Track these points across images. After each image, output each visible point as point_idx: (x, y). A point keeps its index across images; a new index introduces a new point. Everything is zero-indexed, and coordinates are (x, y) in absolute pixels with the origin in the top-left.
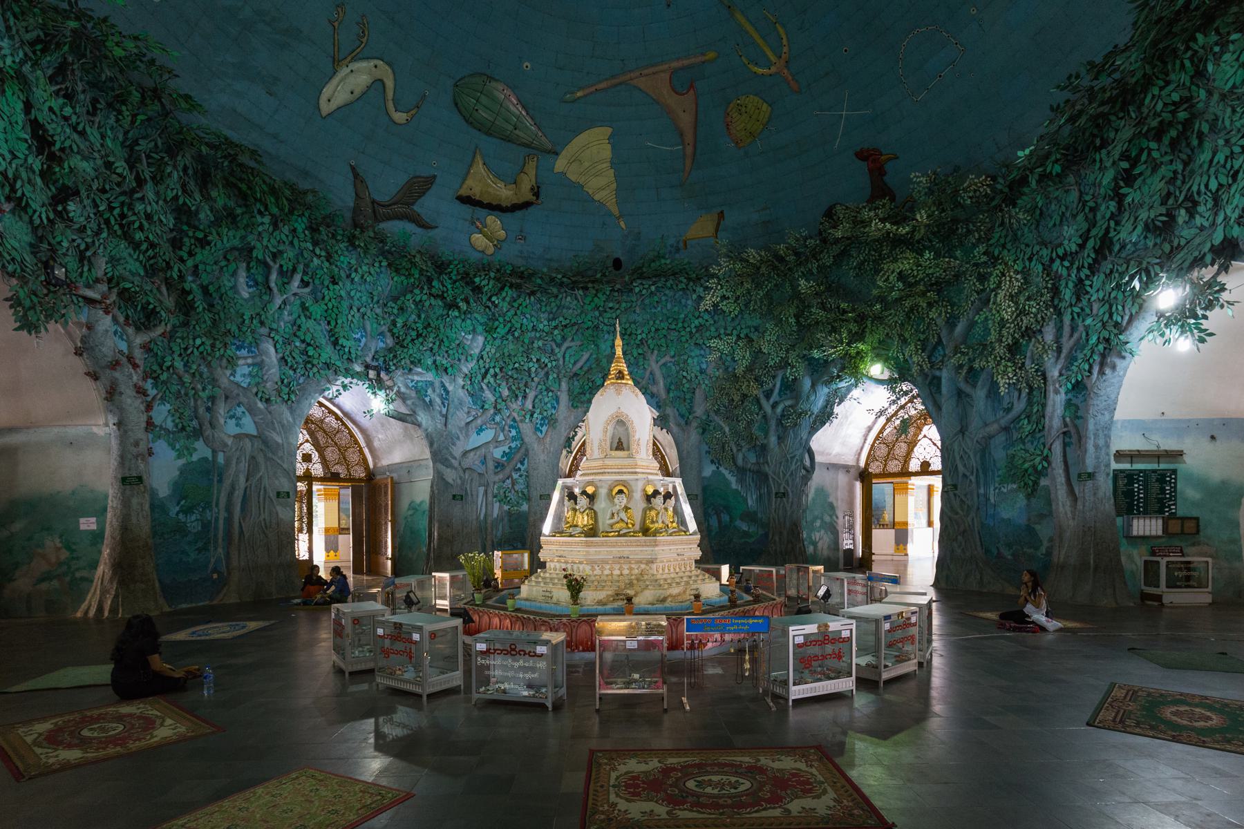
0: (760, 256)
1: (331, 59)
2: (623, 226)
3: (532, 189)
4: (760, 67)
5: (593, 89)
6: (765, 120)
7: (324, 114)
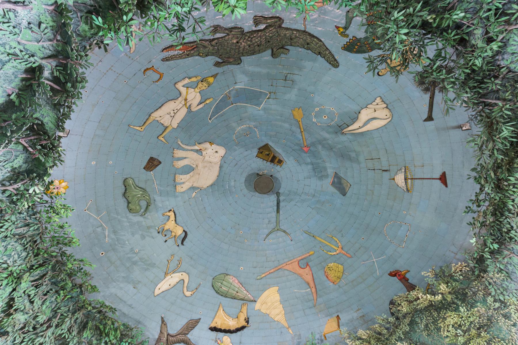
0: (367, 334)
1: (164, 273)
2: (291, 332)
3: (245, 319)
4: (332, 252)
5: (269, 273)
6: (342, 271)
7: (156, 294)
